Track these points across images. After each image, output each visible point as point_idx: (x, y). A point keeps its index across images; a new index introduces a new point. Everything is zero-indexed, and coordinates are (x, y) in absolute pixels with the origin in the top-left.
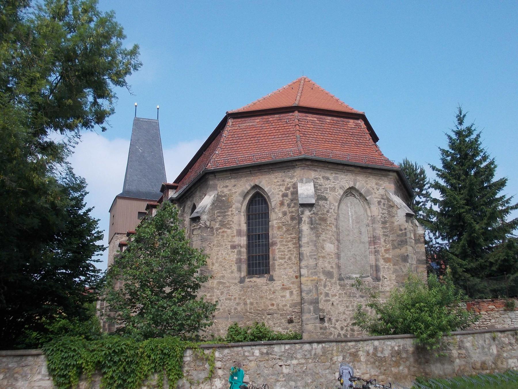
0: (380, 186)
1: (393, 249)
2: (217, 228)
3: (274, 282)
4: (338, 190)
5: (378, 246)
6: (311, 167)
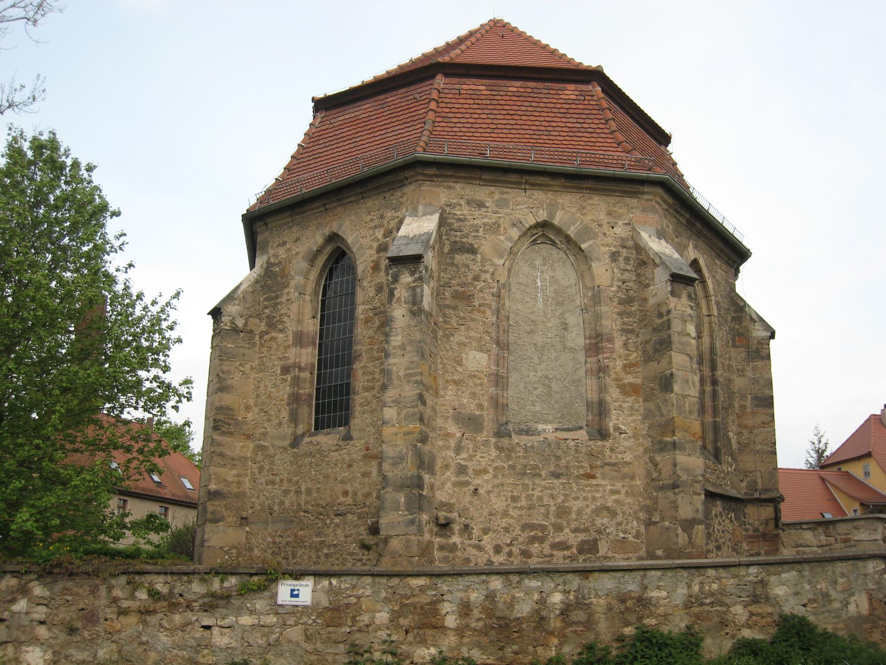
0: (620, 217)
1: (646, 362)
2: (262, 332)
3: (351, 443)
4: (505, 229)
5: (605, 355)
6: (440, 180)
